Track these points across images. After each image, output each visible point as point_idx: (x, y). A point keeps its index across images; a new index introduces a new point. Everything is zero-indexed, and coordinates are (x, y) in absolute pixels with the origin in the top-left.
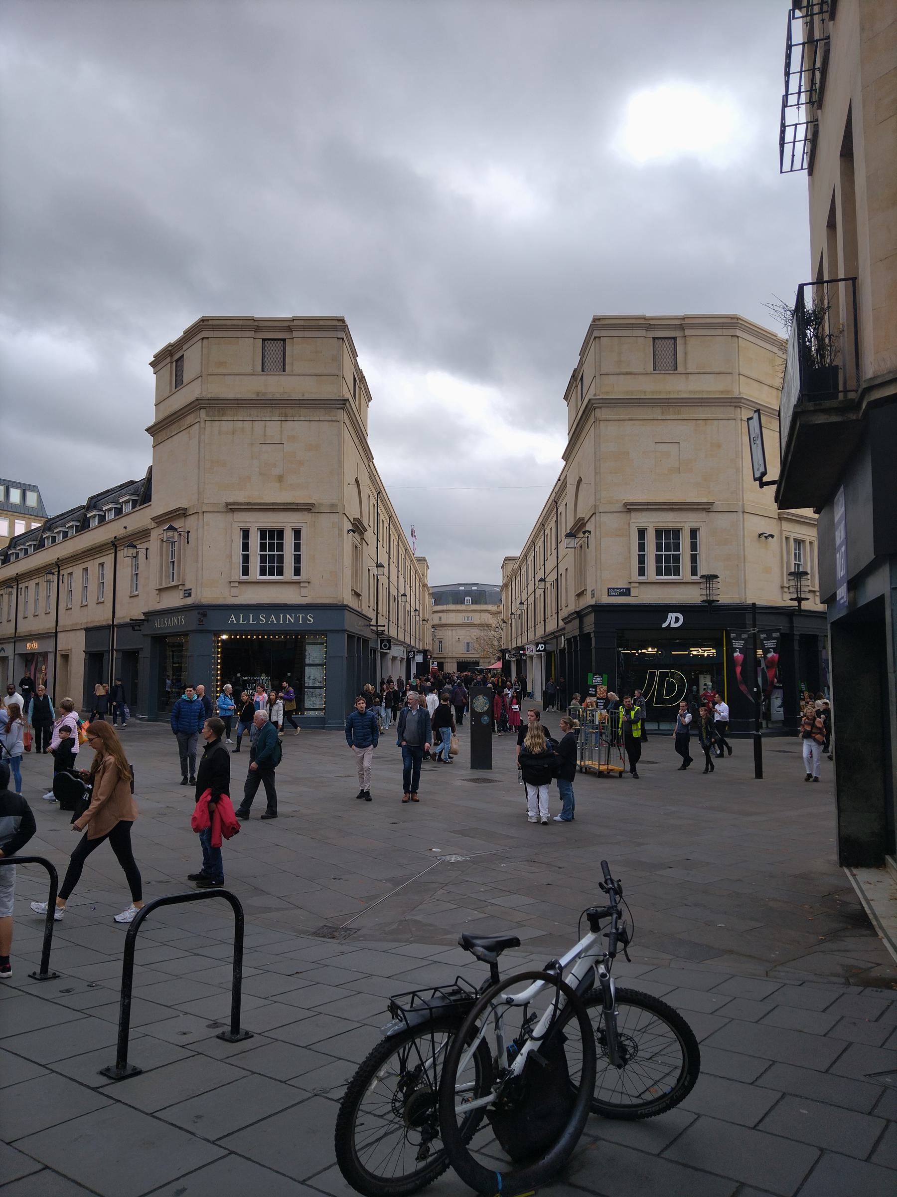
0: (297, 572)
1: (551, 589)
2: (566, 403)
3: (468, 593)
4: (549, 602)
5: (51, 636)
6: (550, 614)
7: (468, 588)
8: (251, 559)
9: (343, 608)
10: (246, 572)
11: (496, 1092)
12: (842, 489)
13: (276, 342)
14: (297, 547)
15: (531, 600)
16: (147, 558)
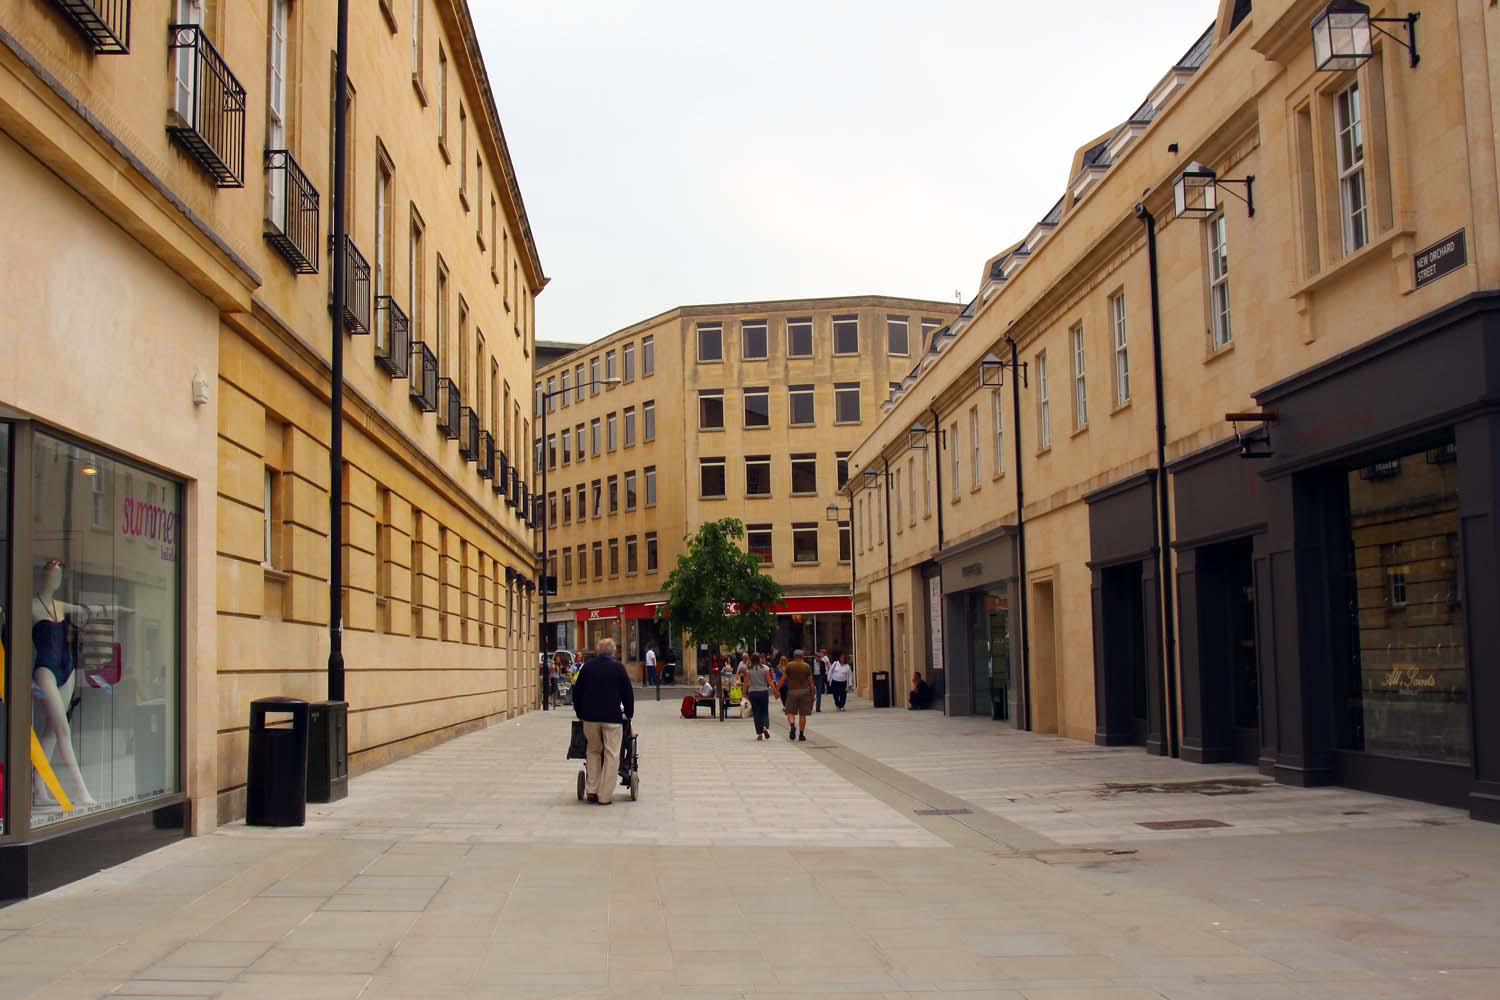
12: (336, 50)
16: (1251, 212)
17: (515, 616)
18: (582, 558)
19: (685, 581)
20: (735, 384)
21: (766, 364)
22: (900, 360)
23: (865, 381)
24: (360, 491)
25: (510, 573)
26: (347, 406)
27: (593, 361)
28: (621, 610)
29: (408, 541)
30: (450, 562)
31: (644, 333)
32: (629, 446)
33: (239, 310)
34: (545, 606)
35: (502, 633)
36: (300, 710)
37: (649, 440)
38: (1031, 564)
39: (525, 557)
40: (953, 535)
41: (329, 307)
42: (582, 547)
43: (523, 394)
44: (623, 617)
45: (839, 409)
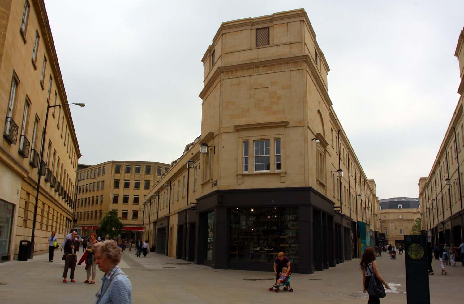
0: (279, 167)
2: (456, 58)
4: (445, 202)
6: (454, 202)
7: (400, 200)
8: (250, 160)
9: (309, 190)
10: (246, 169)
13: (263, 30)
14: (278, 151)
15: (439, 197)
17: (67, 228)
18: (85, 215)
19: (104, 222)
20: (122, 179)
21: (130, 175)
22: (159, 176)
23: (152, 180)
24: (40, 204)
25: (67, 218)
26: (40, 190)
27: (91, 170)
28: (92, 227)
29: (47, 212)
30: (54, 216)
31: (104, 165)
32: (98, 190)
33: (25, 177)
34: (74, 225)
35: (64, 231)
36: (28, 242)
37: (102, 189)
38: (170, 224)
39: (71, 215)
40: (160, 217)
41: (38, 172)
42: (85, 212)
43: (73, 180)
44: (93, 229)
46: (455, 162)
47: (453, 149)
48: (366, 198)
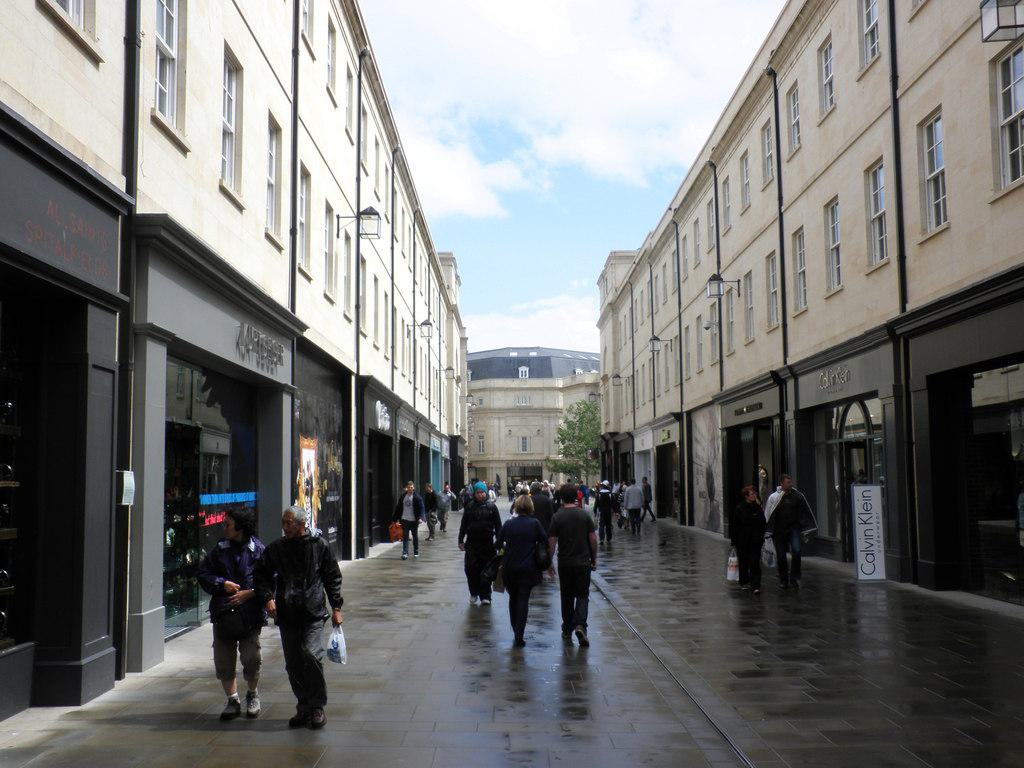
1: (666, 354)
3: (524, 361)
4: (641, 388)
5: (533, 616)
7: (523, 354)
11: (323, 500)
45: (484, 357)
46: (673, 300)
47: (703, 228)
48: (443, 346)
